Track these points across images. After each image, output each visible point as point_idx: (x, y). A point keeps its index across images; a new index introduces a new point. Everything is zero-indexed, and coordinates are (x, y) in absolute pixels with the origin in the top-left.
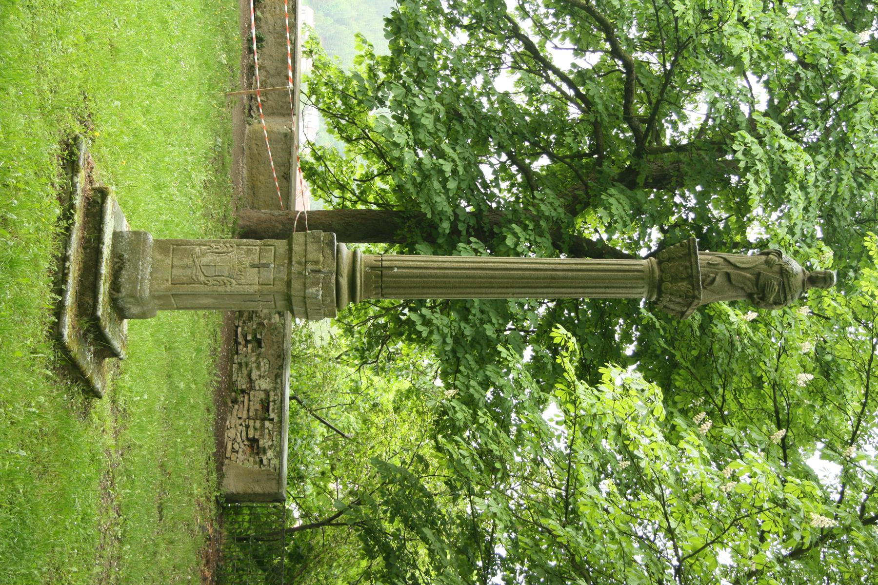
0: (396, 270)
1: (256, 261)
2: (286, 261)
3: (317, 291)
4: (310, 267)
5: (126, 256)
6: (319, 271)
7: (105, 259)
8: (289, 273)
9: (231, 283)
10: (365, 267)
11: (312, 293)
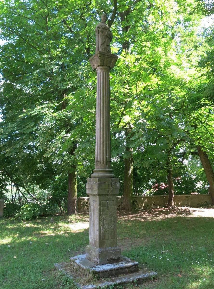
0: (107, 156)
1: (106, 207)
2: (106, 196)
3: (118, 184)
4: (110, 187)
5: (108, 258)
6: (112, 184)
7: (118, 266)
8: (111, 195)
9: (114, 216)
10: (106, 167)
11: (119, 186)
